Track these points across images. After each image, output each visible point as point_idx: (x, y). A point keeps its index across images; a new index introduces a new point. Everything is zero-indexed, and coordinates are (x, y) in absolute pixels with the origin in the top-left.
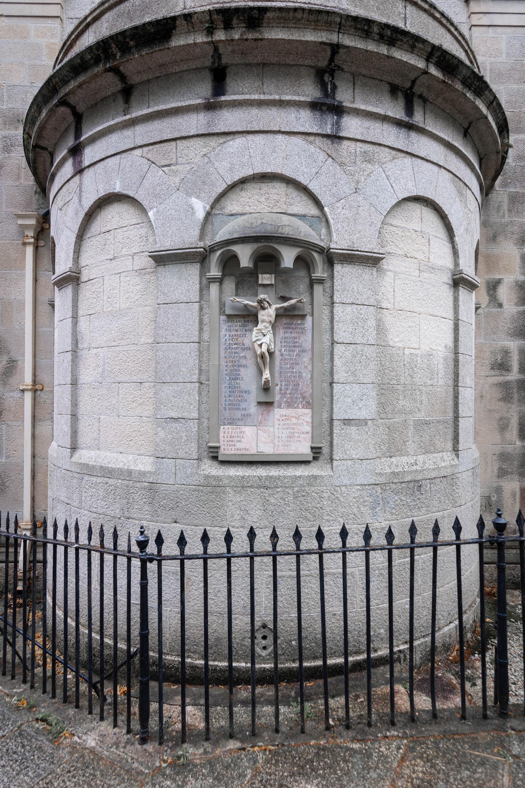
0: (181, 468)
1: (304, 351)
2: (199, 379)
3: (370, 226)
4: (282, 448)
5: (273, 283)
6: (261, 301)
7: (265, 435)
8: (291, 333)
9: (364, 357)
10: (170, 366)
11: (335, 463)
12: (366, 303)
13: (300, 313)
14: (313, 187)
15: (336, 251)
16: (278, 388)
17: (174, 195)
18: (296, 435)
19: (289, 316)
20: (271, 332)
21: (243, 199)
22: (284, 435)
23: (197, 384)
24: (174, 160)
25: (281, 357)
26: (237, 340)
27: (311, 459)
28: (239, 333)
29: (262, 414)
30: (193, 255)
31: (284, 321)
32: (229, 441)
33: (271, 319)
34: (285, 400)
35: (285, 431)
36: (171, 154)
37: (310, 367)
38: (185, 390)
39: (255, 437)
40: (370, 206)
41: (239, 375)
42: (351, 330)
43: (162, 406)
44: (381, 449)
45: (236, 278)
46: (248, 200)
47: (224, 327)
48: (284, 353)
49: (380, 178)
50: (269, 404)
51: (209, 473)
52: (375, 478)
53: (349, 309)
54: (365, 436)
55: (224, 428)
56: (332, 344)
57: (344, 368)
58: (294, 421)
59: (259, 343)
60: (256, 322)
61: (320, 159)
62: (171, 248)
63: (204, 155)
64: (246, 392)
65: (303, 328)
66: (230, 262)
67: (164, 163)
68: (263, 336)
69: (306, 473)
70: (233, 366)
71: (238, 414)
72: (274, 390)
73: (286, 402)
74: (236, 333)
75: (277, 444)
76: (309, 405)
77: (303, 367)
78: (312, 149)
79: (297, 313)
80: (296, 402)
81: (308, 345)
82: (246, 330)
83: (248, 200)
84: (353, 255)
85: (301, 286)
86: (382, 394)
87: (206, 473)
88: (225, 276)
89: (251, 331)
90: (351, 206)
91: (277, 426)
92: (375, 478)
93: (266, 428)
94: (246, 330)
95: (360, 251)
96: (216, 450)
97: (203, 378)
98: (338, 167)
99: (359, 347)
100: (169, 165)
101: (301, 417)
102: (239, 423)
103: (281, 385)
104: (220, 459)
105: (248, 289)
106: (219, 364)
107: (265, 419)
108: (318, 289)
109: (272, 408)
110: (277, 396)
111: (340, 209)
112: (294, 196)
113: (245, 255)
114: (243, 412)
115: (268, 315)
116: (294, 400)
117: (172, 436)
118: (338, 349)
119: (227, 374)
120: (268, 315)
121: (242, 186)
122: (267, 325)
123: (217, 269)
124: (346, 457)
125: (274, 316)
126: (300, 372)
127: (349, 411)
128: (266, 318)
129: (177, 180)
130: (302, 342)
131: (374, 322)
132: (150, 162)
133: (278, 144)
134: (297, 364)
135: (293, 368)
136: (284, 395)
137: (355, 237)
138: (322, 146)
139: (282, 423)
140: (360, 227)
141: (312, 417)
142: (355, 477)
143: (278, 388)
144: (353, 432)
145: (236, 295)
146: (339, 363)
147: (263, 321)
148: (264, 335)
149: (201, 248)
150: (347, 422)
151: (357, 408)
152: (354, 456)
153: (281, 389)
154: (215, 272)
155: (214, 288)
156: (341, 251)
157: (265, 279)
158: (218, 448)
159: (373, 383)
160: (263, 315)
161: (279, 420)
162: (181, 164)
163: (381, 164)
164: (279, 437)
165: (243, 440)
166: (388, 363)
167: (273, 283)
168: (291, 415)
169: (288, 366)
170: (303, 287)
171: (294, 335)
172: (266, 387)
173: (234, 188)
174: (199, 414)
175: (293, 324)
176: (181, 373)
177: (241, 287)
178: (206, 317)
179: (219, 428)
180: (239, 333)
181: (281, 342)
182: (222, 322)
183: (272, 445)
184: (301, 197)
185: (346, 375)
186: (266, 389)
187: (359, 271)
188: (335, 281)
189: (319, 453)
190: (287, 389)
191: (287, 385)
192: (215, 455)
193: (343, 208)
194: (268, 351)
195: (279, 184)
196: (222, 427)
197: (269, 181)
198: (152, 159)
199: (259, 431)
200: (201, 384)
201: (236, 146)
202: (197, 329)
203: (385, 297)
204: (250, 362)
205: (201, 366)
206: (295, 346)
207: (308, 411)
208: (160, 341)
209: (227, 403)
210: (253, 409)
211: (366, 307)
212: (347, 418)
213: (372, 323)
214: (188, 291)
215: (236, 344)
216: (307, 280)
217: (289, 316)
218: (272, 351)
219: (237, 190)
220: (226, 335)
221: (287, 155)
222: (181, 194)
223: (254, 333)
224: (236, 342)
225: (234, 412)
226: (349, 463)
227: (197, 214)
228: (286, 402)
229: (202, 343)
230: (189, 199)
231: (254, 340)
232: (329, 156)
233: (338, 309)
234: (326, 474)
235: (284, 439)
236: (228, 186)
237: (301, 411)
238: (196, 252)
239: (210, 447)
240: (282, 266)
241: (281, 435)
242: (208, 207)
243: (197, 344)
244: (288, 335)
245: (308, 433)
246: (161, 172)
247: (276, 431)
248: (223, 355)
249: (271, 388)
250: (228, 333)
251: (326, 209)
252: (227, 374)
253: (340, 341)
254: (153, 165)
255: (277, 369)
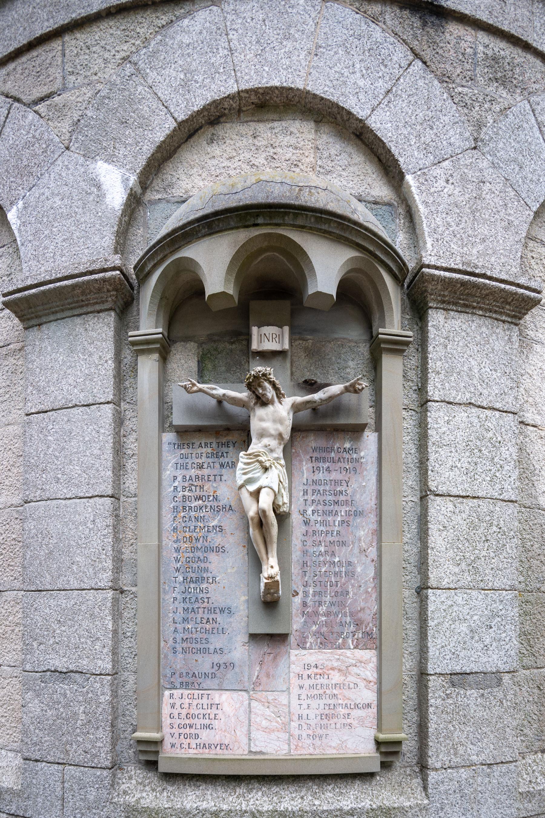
0: (76, 787)
1: (358, 514)
2: (115, 580)
3: (506, 229)
4: (309, 741)
5: (287, 346)
6: (256, 377)
7: (268, 712)
8: (328, 470)
9: (495, 528)
10: (51, 553)
11: (433, 777)
12: (498, 405)
13: (352, 421)
14: (381, 124)
15: (437, 272)
16: (297, 600)
17: (59, 162)
18: (343, 711)
19: (323, 428)
20: (283, 462)
21: (215, 162)
22: (312, 713)
23: (110, 594)
24: (59, 81)
25: (304, 528)
26: (202, 487)
27: (376, 767)
28: (206, 472)
29: (261, 663)
30: (99, 290)
31: (313, 442)
32: (185, 726)
33: (281, 428)
34: (314, 628)
35: (314, 703)
36: (51, 70)
37: (373, 552)
38: (83, 608)
39: (243, 717)
40: (505, 185)
41: (206, 570)
42: (466, 465)
43: (35, 644)
44: (526, 735)
45: (200, 344)
46: (226, 163)
47: (171, 458)
48: (313, 518)
49: (525, 125)
50: (277, 639)
51: (138, 801)
52: (517, 805)
53: (462, 415)
54: (497, 710)
55: (171, 696)
56: (423, 498)
57: (451, 553)
58: (336, 677)
59: (252, 488)
60: (247, 442)
61: (395, 58)
62: (48, 278)
63: (124, 59)
64: (222, 611)
65: (357, 460)
66: (185, 299)
67: (37, 93)
68: (263, 474)
69: (367, 804)
70: (194, 549)
71: (205, 663)
72: (289, 605)
73: (318, 633)
74: (200, 473)
75: (296, 732)
76: (373, 640)
77: (356, 551)
78: (377, 33)
79: (342, 421)
80: (340, 634)
81: (366, 499)
82: (222, 466)
83: (226, 163)
84: (475, 285)
85: (351, 364)
86: (526, 614)
87: (132, 800)
88: (175, 342)
89: (234, 465)
90: (464, 179)
91: (295, 691)
92: (517, 805)
93: (271, 696)
94: (222, 466)
95: (490, 278)
96: (152, 748)
97: (125, 580)
98: (436, 82)
99: (484, 506)
100: (49, 96)
101: (354, 670)
102: (208, 683)
103: (306, 593)
104: (163, 767)
105: (228, 370)
106: (160, 547)
107: (268, 675)
108: (392, 368)
109: (283, 649)
110: (295, 619)
111: (442, 182)
112: (333, 152)
113: (215, 264)
114: (217, 658)
115: (274, 418)
116: (336, 629)
117: (54, 712)
118: (438, 509)
119: (178, 570)
120: (274, 418)
121: (211, 130)
122: (273, 443)
123: (153, 319)
124: (456, 760)
125: (289, 423)
126: (350, 563)
127: (462, 655)
128: (268, 425)
129: (65, 126)
130: (355, 492)
131: (514, 450)
132: (10, 100)
133: (295, 18)
134: (344, 544)
135: (333, 554)
136: (311, 616)
137: (474, 251)
138: (398, 29)
139: (307, 683)
140: (484, 230)
141: (379, 669)
142: (476, 808)
143: (297, 600)
144: (472, 702)
145: (201, 378)
146: (440, 541)
147: (262, 434)
148: (266, 469)
149: (114, 269)
150: (458, 679)
151: (480, 646)
152: (474, 758)
153: (305, 604)
154: (148, 324)
155: (148, 368)
156: (447, 274)
157: (268, 338)
158: (158, 743)
159: (513, 588)
160: (261, 420)
161: (300, 676)
162: (74, 88)
163: (528, 93)
164: (300, 717)
165: (215, 723)
166: (536, 546)
167: (287, 346)
168: (329, 664)
169: (322, 549)
170: (355, 367)
171: (334, 476)
172: (269, 598)
173: (196, 137)
174: (115, 662)
175: (332, 449)
176: (75, 567)
177: (210, 366)
178: (132, 438)
179: (160, 696)
180: (206, 472)
181: (305, 492)
182: (165, 447)
183: (284, 736)
184: (350, 155)
185: (457, 570)
186: (270, 603)
187: (484, 329)
188: (430, 349)
189: (396, 753)
190: (320, 604)
191: (320, 593)
192: (152, 758)
193: (447, 181)
194: (276, 508)
195: (297, 123)
196: (167, 693)
197: (276, 116)
198: (13, 93)
199: (254, 704)
200: (122, 592)
201: (198, 28)
202: (110, 464)
203: (530, 400)
204: (231, 539)
205: (120, 552)
206: (336, 503)
207: (370, 655)
208: (31, 497)
209: (179, 637)
210: (239, 650)
211: (497, 414)
212: (458, 669)
213: (509, 451)
214: (89, 377)
215: (200, 498)
216: (364, 349)
217: (323, 428)
218: (285, 509)
219: (201, 140)
220: (175, 478)
221: (318, 47)
222: (75, 156)
223: (240, 465)
224: (198, 493)
225: (196, 657)
226: (464, 774)
227: (108, 199)
228: (318, 633)
229: (123, 499)
230: (92, 166)
231: (240, 482)
232: (417, 56)
233: (437, 415)
234: (412, 802)
235: (313, 723)
236: (181, 124)
237: (353, 655)
238: (104, 280)
239: (140, 742)
240: (311, 291)
241: (305, 713)
242: (133, 179)
243: (108, 501)
244: (320, 476)
245: (369, 706)
246: (31, 116)
247: (295, 702)
248: (168, 524)
249: (282, 601)
250: (179, 473)
251: (409, 178)
252: (178, 570)
253: (442, 489)
254: (16, 104)
255: (296, 555)
